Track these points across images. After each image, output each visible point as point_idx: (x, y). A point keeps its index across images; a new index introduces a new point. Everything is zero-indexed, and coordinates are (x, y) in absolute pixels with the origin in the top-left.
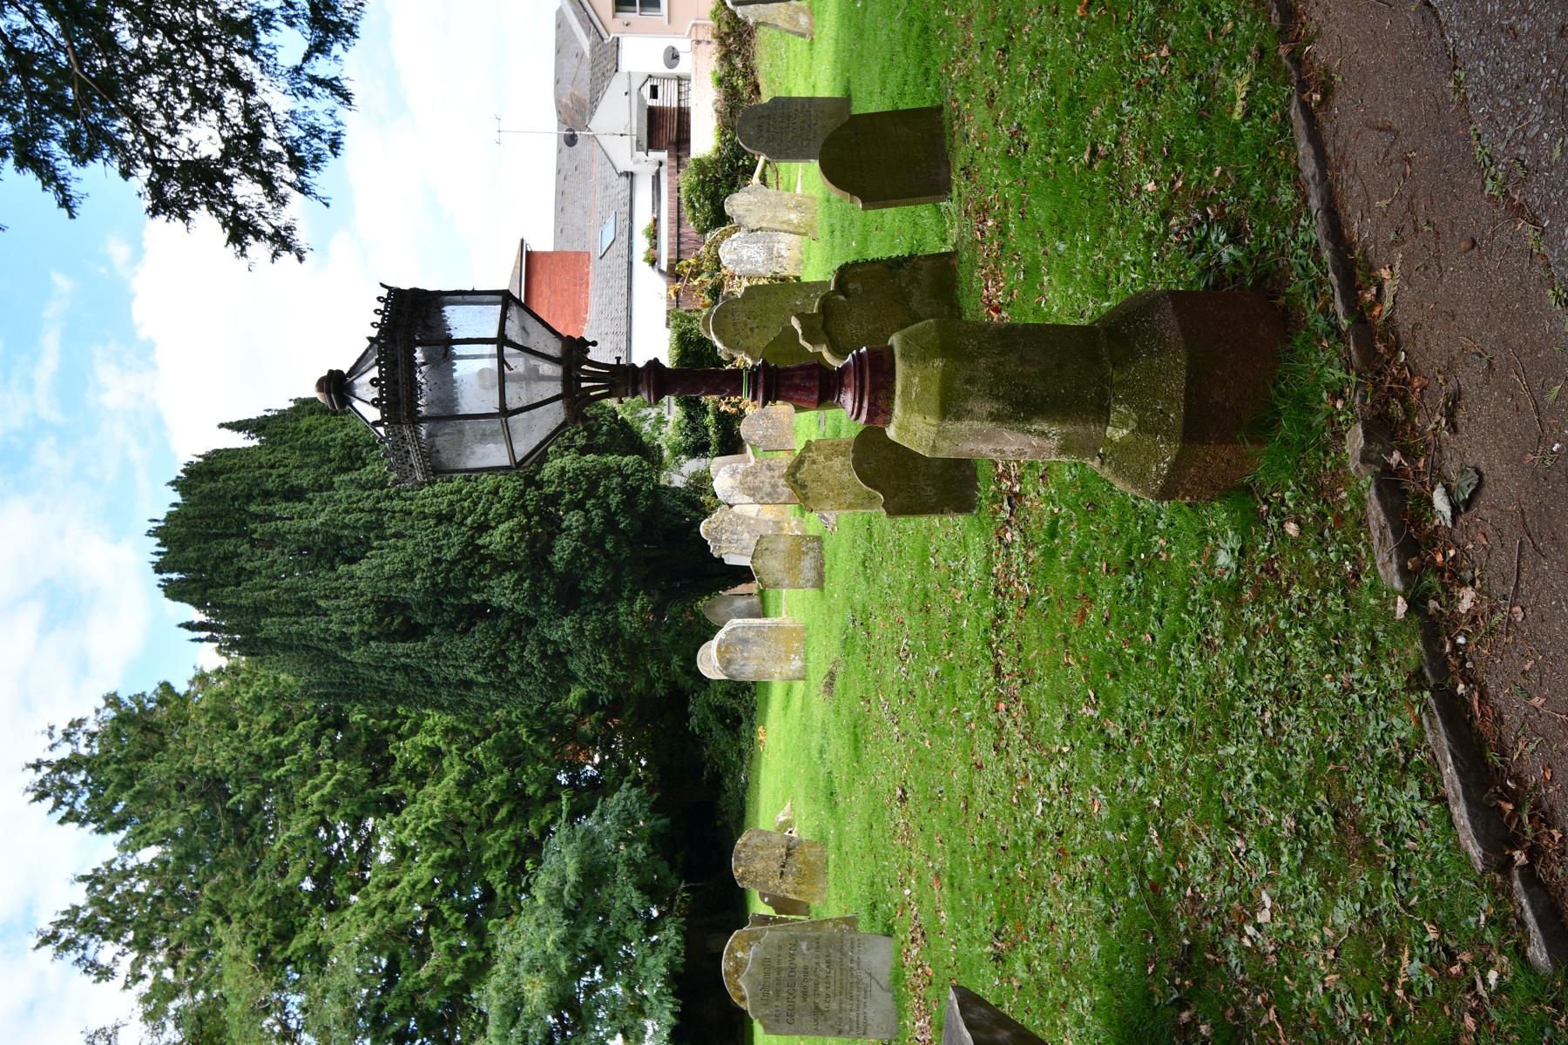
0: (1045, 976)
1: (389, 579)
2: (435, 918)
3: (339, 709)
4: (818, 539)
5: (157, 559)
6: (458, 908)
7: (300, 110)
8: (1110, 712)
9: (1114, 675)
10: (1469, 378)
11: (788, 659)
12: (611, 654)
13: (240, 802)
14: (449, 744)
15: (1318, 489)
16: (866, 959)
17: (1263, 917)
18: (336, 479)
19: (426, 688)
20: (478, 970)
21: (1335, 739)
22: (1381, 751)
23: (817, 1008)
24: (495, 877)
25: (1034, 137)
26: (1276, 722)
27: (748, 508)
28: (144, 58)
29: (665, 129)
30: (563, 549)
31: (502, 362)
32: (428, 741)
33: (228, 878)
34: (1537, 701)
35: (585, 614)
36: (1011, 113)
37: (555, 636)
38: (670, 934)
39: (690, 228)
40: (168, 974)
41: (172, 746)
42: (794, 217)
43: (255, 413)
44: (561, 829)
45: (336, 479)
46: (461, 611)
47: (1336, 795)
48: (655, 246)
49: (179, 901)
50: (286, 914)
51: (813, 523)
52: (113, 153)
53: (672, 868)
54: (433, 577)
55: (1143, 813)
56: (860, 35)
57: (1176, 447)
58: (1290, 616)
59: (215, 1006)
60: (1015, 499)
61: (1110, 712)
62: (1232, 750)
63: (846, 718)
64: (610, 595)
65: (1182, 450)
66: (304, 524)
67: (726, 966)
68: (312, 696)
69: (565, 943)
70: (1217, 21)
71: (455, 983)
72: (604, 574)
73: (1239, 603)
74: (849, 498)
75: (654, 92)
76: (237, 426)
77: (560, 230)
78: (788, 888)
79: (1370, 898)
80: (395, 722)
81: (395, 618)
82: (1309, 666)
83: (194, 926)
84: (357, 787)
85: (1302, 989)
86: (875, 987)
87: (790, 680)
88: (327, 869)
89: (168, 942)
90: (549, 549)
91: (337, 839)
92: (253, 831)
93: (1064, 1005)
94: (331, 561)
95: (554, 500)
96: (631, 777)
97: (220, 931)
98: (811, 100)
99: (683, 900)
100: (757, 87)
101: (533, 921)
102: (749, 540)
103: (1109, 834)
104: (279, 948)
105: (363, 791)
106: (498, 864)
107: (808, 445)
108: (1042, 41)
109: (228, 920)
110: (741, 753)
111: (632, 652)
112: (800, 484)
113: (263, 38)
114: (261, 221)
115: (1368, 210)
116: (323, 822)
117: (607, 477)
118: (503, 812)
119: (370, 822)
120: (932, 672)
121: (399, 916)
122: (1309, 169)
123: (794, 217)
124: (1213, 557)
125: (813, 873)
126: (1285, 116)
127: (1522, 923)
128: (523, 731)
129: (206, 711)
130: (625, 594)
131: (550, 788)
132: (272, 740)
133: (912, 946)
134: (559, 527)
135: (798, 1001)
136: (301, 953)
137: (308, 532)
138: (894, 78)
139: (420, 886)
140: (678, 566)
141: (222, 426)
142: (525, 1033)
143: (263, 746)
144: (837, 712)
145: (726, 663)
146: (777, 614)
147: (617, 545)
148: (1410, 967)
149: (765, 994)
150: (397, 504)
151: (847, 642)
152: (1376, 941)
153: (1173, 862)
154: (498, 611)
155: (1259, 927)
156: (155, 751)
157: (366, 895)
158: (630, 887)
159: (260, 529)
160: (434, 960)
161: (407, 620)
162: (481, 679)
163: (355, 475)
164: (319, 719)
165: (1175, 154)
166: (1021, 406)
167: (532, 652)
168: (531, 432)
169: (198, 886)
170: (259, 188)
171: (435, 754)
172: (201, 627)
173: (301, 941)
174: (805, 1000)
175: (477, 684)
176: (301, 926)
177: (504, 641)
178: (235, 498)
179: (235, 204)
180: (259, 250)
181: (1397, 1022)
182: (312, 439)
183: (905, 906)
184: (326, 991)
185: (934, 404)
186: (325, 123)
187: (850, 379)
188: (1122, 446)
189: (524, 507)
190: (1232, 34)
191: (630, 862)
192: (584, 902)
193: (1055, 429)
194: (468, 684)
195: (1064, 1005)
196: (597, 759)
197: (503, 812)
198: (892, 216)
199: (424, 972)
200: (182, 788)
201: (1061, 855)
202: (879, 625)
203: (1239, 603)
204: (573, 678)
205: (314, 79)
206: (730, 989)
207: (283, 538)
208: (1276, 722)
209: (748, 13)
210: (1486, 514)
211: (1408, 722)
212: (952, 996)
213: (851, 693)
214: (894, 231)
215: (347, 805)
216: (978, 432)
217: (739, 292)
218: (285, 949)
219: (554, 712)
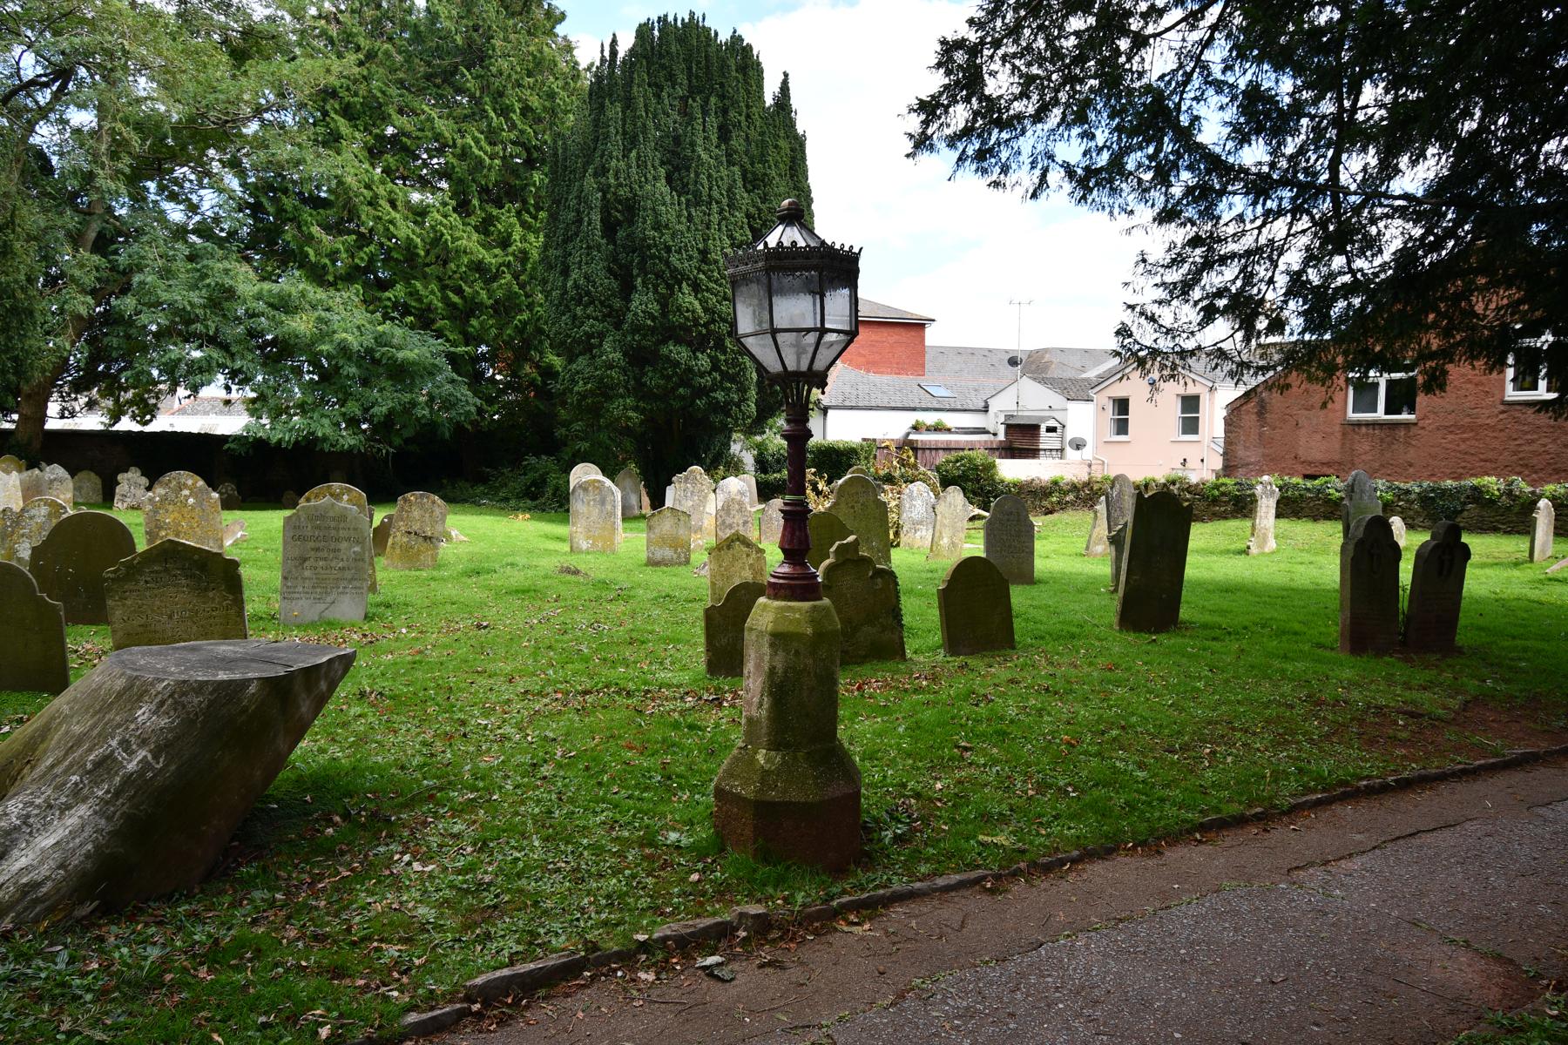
0: (353, 727)
1: (654, 209)
2: (364, 240)
3: (543, 162)
4: (687, 562)
5: (671, 19)
6: (372, 259)
7: (1021, 159)
8: (560, 766)
9: (587, 768)
10: (795, 973)
13: (463, 76)
14: (513, 254)
15: (723, 892)
16: (346, 599)
17: (417, 866)
18: (736, 169)
19: (563, 236)
20: (317, 275)
21: (549, 904)
22: (542, 931)
23: (305, 560)
25: (982, 709)
26: (558, 870)
27: (712, 505)
28: (1059, 37)
29: (1022, 438)
30: (680, 353)
31: (808, 330)
32: (516, 236)
34: (580, 1015)
35: (624, 371)
36: (1002, 695)
37: (606, 346)
38: (348, 440)
39: (941, 458)
41: (511, 22)
42: (945, 541)
43: (795, 102)
44: (438, 345)
45: (736, 169)
46: (627, 268)
47: (508, 907)
48: (928, 429)
49: (377, 22)
50: (367, 113)
51: (699, 557)
52: (989, 12)
53: (407, 441)
55: (486, 789)
56: (1080, 591)
57: (751, 796)
58: (634, 876)
60: (718, 703)
61: (560, 766)
62: (536, 843)
63: (541, 583)
64: (640, 392)
65: (749, 801)
66: (700, 141)
67: (336, 486)
68: (555, 142)
69: (344, 349)
70: (1048, 825)
71: (307, 255)
72: (658, 387)
73: (642, 846)
74: (719, 584)
75: (1051, 430)
76: (785, 87)
77: (942, 351)
78: (397, 537)
79: (439, 928)
81: (622, 213)
82: (599, 889)
84: (478, 176)
85: (367, 891)
86: (323, 606)
87: (570, 540)
88: (405, 149)
89: (341, 12)
90: (679, 342)
91: (431, 158)
93: (333, 740)
94: (669, 162)
95: (720, 346)
97: (352, 58)
98: (1032, 553)
99: (379, 450)
100: (1051, 512)
102: (686, 505)
105: (473, 180)
106: (411, 294)
107: (762, 551)
108: (1049, 714)
109: (361, 64)
110: (506, 500)
111: (593, 407)
112: (732, 544)
113: (1076, 131)
114: (936, 126)
115: (909, 916)
117: (738, 390)
118: (455, 299)
119: (444, 185)
120: (583, 647)
121: (365, 210)
122: (940, 882)
123: (945, 541)
124: (674, 829)
125: (410, 558)
126: (978, 867)
127: (432, 1008)
128: (525, 316)
129: (541, 52)
130: (641, 404)
132: (517, 106)
134: (697, 349)
135: (312, 544)
136: (332, 125)
137: (693, 144)
138: (1039, 614)
140: (663, 448)
141: (786, 75)
143: (512, 99)
144: (546, 577)
145: (584, 487)
146: (625, 529)
147: (682, 398)
148: (393, 951)
150: (715, 218)
151: (604, 584)
152: (412, 932)
153: (451, 809)
154: (628, 300)
155: (409, 864)
156: (506, 8)
159: (695, 105)
160: (326, 239)
161: (619, 223)
162: (570, 284)
163: (740, 183)
165: (959, 800)
166: (779, 689)
167: (592, 326)
168: (761, 349)
169: (390, 39)
170: (961, 125)
171: (505, 243)
172: (614, 53)
173: (343, 126)
175: (565, 280)
176: (356, 126)
177: (602, 303)
178: (722, 85)
179: (949, 106)
180: (914, 123)
181: (354, 943)
182: (771, 150)
183: (392, 629)
184: (299, 145)
185: (782, 628)
186: (1009, 180)
187: (799, 571)
188: (753, 760)
189: (713, 321)
190: (1038, 834)
192: (377, 365)
193: (764, 713)
194: (566, 272)
195: (333, 740)
196: (498, 377)
197: (455, 299)
198: (934, 614)
199: (316, 230)
200: (476, 28)
201: (449, 737)
202: (619, 608)
203: (642, 846)
204: (571, 360)
205: (1045, 171)
207: (688, 123)
208: (558, 870)
209: (1101, 507)
210: (704, 985)
211: (562, 944)
213: (562, 587)
214: (921, 615)
216: (762, 659)
217: (882, 497)
218: (336, 112)
219: (541, 342)
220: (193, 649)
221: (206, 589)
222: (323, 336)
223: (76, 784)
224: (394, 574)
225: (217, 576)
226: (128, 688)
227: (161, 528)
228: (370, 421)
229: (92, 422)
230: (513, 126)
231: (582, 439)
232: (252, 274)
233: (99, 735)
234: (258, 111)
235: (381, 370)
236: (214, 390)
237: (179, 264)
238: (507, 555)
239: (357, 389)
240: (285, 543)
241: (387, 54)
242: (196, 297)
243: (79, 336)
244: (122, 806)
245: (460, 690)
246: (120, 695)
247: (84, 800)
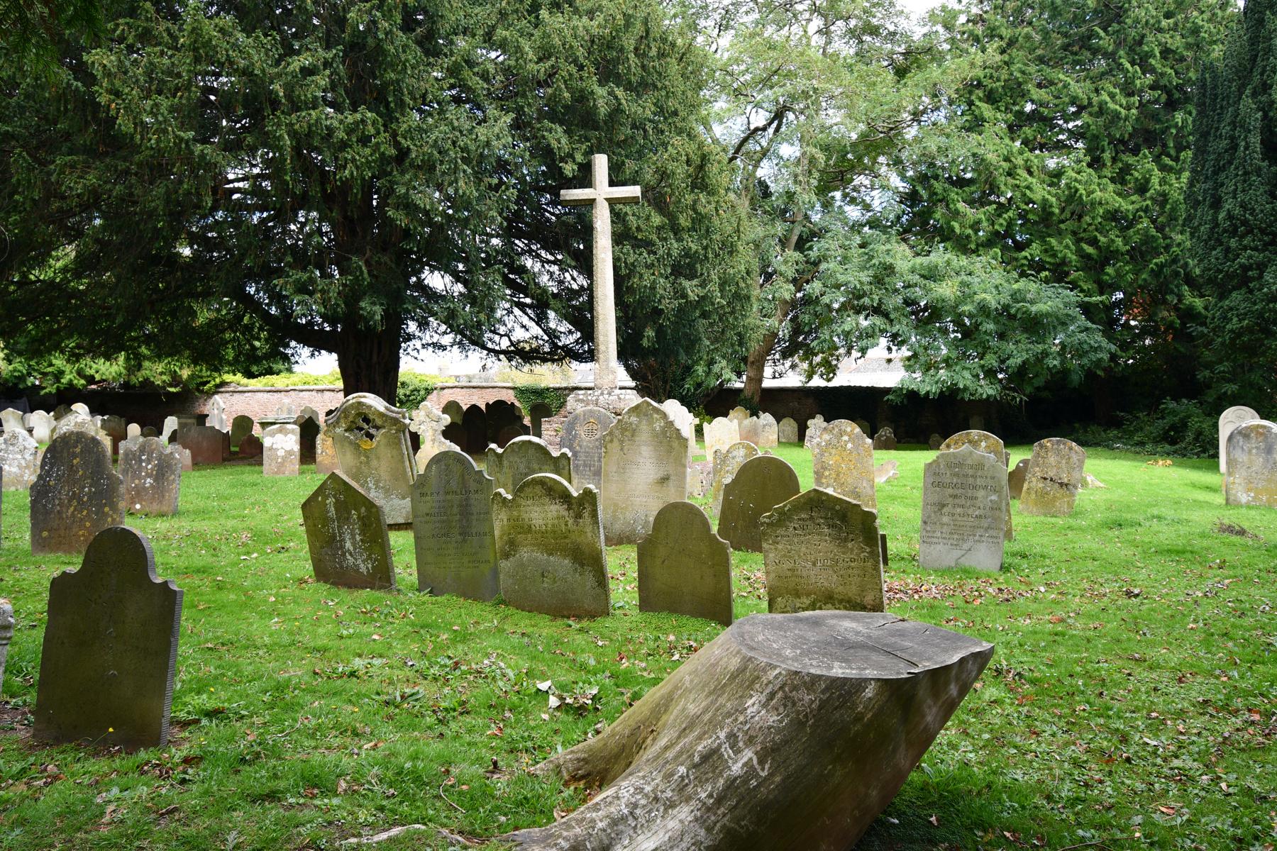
0: (987, 717)
3: (1187, 99)
6: (1010, 223)
11: (1250, 490)
12: (1249, 330)
14: (1152, 198)
19: (1212, 172)
20: (963, 246)
23: (944, 506)
24: (1035, 250)
32: (1155, 181)
33: (1037, 44)
38: (987, 390)
40: (962, 19)
44: (1072, 296)
53: (1038, 389)
59: (938, 58)
63: (1198, 543)
67: (974, 433)
69: (983, 309)
78: (1032, 482)
80: (1173, 152)
83: (999, 27)
86: (959, 553)
91: (1066, 122)
92: (1076, 54)
96: (1119, 353)
97: (993, 47)
99: (1014, 398)
101: (998, 281)
103: (1138, 819)
104: (981, 95)
106: (1046, 251)
110: (1142, 444)
116: (1081, 108)
118: (1090, 250)
125: (1045, 504)
128: (1162, 259)
131: (1110, 286)
133: (995, 587)
135: (950, 491)
139: (1028, 192)
142: (916, 285)
143: (1152, 44)
144: (1203, 535)
149: (956, 465)
157: (1021, 153)
158: (1026, 356)
162: (1222, 216)
164: (1176, 87)
167: (1250, 257)
169: (1030, 23)
171: (1142, 189)
173: (986, 110)
176: (998, 108)
177: (1262, 231)
184: (948, 136)
191: (1045, 354)
192: (1015, 320)
194: (1216, 204)
196: (1133, 323)
197: (1090, 250)
199: (961, 206)
201: (1107, 758)
206: (955, 436)
212: (986, 646)
215: (1096, 124)
218: (980, 99)
220: (816, 623)
221: (846, 540)
222: (965, 298)
223: (682, 777)
224: (1029, 520)
225: (853, 525)
226: (741, 670)
227: (825, 469)
228: (1006, 372)
229: (793, 380)
231: (1229, 381)
232: (908, 252)
233: (710, 721)
234: (916, 116)
235: (1016, 324)
236: (879, 350)
237: (853, 251)
238: (1149, 505)
239: (994, 343)
240: (926, 488)
241: (1028, 37)
242: (865, 277)
243: (786, 315)
244: (723, 817)
245: (1117, 684)
246: (733, 677)
247: (688, 799)
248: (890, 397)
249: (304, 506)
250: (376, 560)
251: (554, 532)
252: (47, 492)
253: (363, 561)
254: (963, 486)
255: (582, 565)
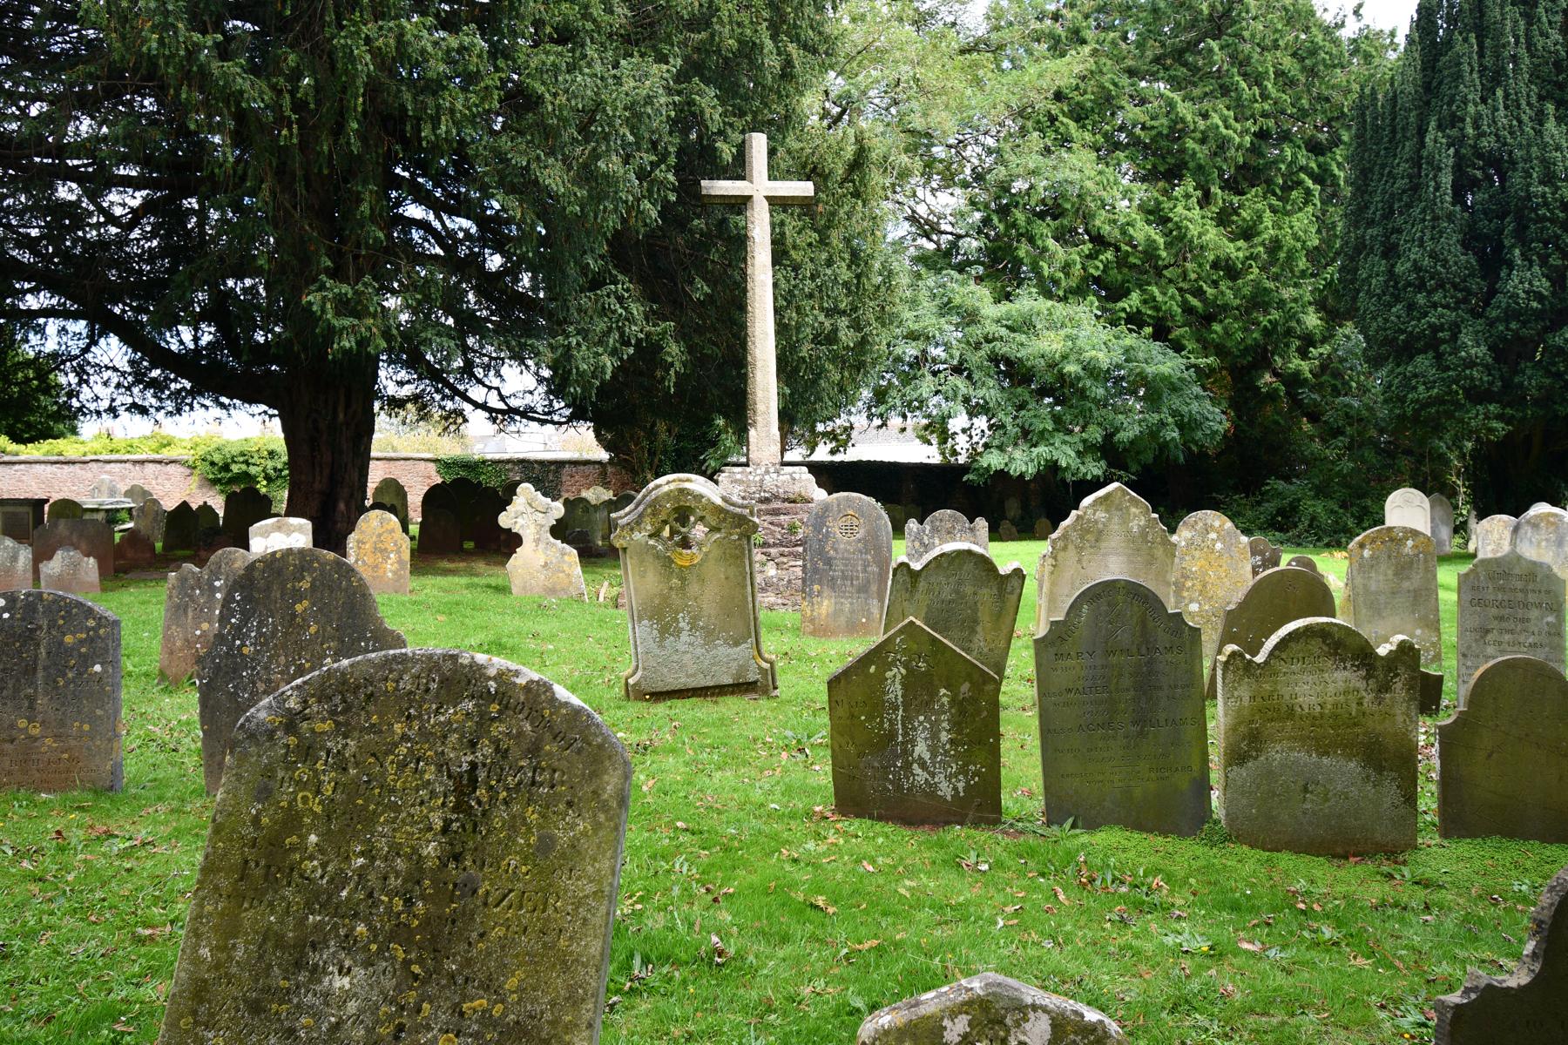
12: (1438, 400)
23: (1488, 631)
35: (1487, 367)
54: (1546, 204)
69: (1091, 370)
118: (1194, 302)
130: (1508, 411)
135: (1494, 611)
174: (1496, 618)
177: (1455, 286)
194: (1391, 252)
197: (1194, 302)
218: (1064, 114)
227: (1187, 578)
230: (1265, 96)
248: (971, 477)
249: (834, 683)
250: (975, 774)
251: (1336, 716)
252: (236, 670)
253: (949, 778)
254: (1510, 604)
255: (1380, 769)
